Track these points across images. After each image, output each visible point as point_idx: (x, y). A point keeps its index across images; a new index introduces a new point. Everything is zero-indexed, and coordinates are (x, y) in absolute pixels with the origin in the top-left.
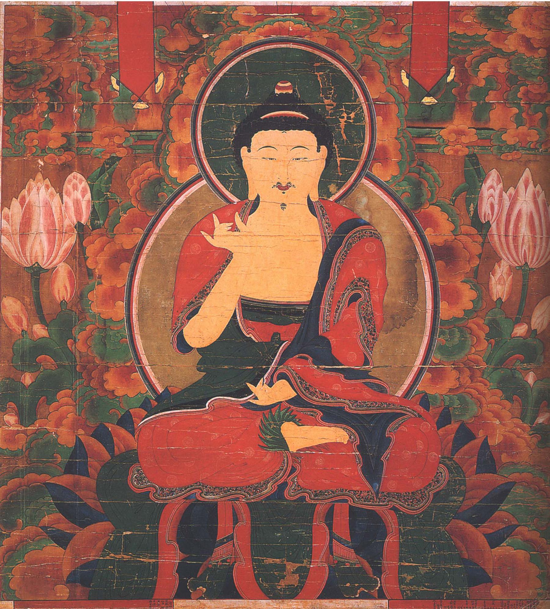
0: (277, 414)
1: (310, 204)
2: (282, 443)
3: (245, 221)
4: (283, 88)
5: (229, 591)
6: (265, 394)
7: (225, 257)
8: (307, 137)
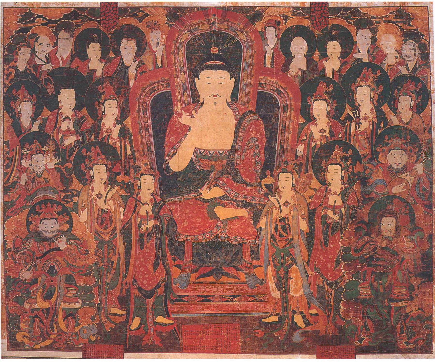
0: (214, 203)
1: (228, 103)
2: (216, 217)
3: (196, 112)
4: (214, 50)
5: (175, 13)
6: (208, 193)
7: (188, 128)
8: (225, 74)
